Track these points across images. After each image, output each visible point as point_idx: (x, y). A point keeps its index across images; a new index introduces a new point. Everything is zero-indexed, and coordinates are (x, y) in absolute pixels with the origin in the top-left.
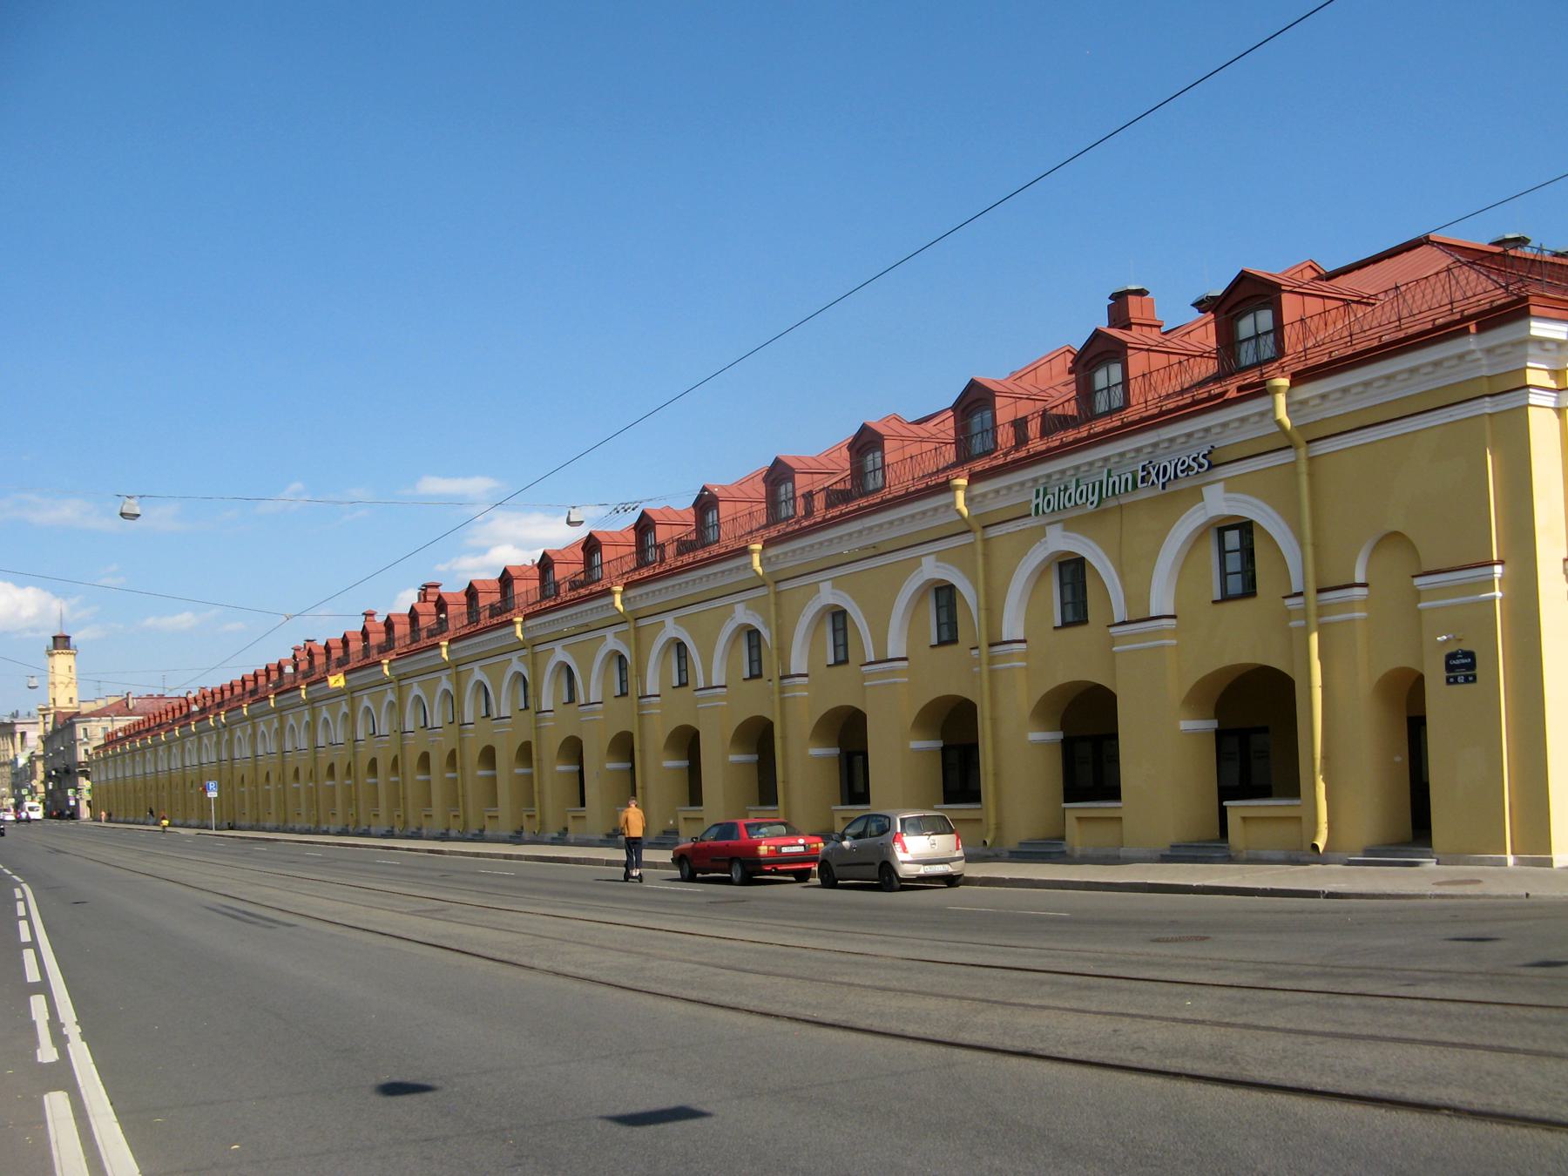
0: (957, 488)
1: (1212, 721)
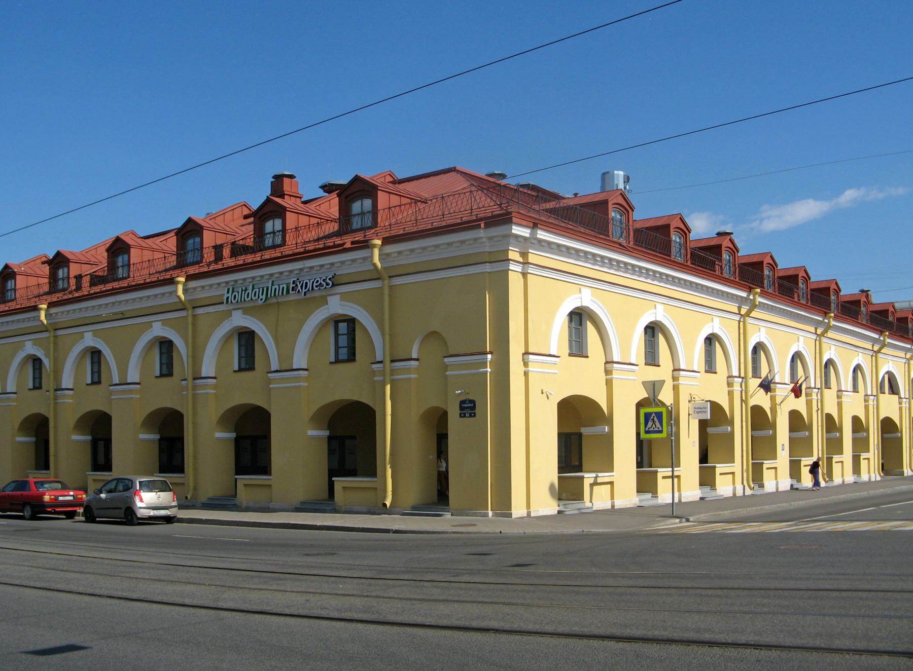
0: (178, 282)
1: (326, 431)
